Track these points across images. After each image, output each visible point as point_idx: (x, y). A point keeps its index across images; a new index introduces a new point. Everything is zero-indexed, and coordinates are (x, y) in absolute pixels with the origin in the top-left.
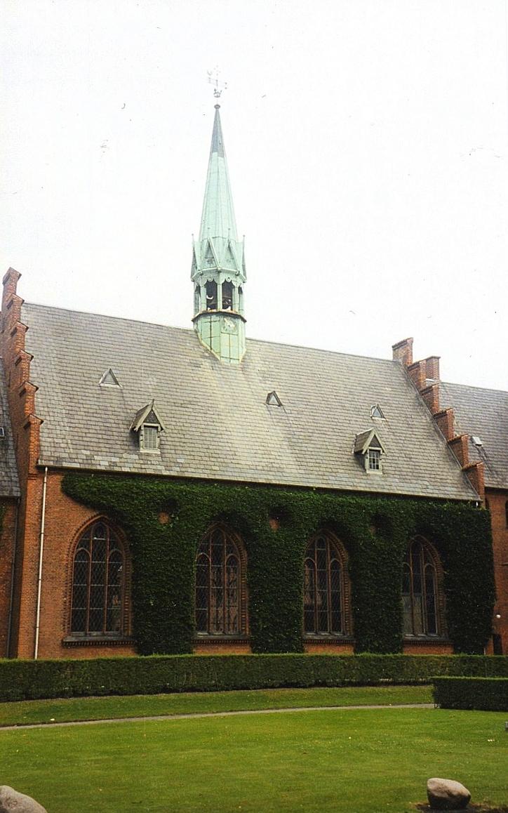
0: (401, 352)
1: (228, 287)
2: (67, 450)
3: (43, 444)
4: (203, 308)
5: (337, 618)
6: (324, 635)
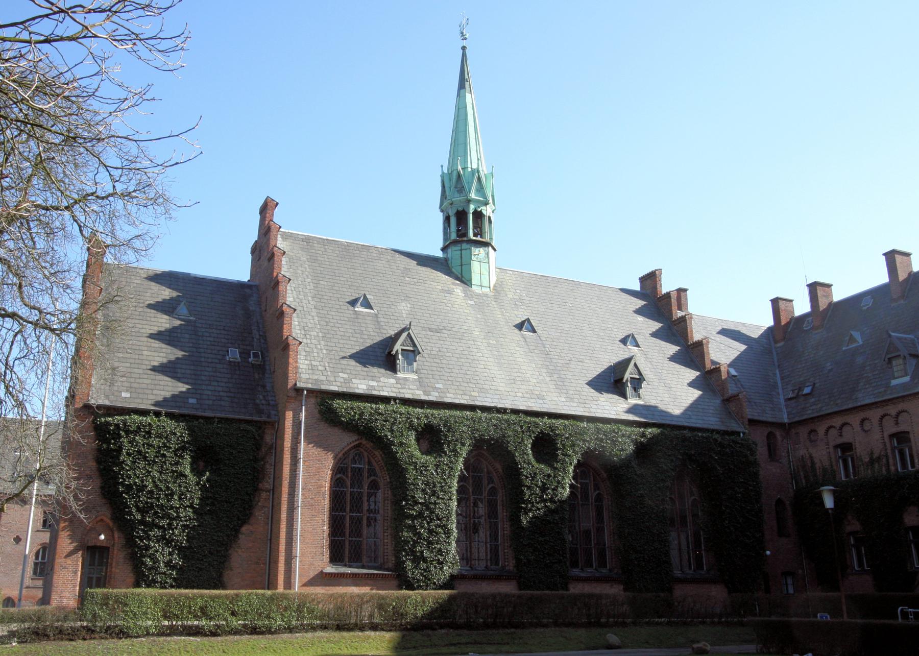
0: (649, 282)
1: (478, 215)
2: (325, 373)
3: (301, 366)
4: (453, 236)
5: (602, 555)
6: (589, 572)
